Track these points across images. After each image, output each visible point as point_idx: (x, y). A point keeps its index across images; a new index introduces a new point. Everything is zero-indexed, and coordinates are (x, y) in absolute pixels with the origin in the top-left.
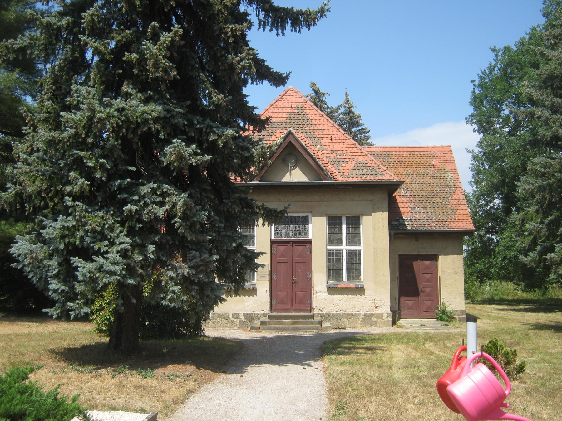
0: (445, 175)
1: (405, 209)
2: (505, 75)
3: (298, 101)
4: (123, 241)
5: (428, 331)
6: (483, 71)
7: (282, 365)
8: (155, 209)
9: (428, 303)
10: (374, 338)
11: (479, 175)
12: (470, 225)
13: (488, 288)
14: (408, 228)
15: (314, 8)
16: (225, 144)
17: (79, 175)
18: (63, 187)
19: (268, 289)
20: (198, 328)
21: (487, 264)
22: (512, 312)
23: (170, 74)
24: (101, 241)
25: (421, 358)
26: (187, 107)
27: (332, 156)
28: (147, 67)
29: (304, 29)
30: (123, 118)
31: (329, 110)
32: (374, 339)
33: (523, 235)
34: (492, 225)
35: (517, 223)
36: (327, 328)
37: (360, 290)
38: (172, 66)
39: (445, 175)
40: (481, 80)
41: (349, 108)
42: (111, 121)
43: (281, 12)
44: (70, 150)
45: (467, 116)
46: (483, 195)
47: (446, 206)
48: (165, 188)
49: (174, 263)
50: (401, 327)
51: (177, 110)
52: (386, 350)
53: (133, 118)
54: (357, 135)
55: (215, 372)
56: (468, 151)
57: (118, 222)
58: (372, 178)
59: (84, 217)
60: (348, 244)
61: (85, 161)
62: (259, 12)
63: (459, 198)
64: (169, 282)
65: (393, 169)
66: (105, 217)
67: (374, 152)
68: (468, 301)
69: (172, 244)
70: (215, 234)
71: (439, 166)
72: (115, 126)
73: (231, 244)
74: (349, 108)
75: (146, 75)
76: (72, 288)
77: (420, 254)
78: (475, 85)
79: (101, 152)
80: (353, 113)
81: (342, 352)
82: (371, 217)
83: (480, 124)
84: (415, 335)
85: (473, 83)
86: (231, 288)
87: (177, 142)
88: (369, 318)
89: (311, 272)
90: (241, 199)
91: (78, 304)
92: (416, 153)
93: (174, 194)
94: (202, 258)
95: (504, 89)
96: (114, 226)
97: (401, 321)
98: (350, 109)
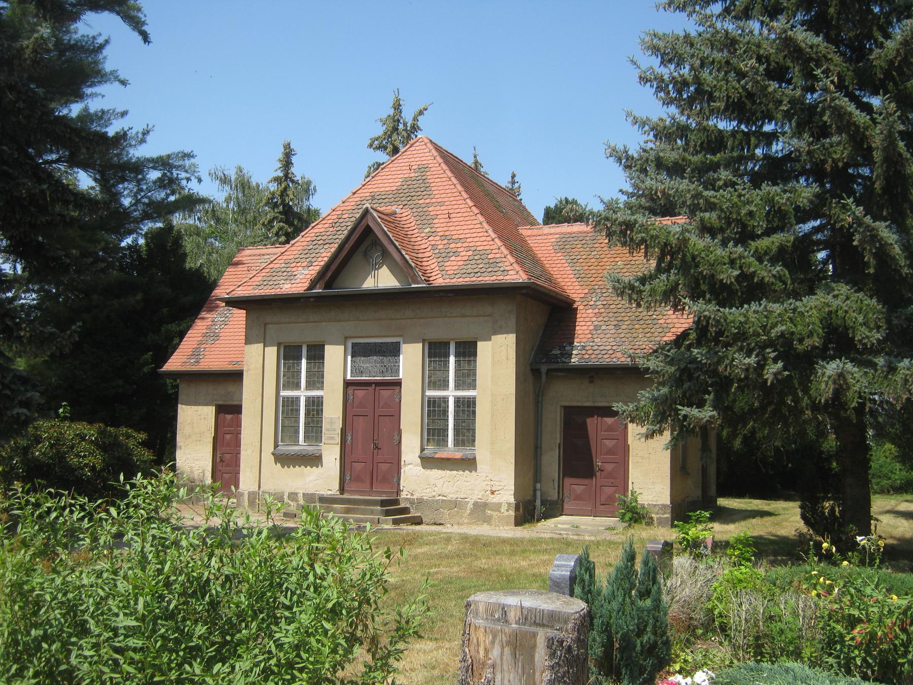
9: (608, 490)
19: (338, 457)
37: (469, 464)
47: (655, 322)
60: (458, 387)
67: (574, 233)
77: (596, 405)
82: (489, 343)
88: (481, 510)
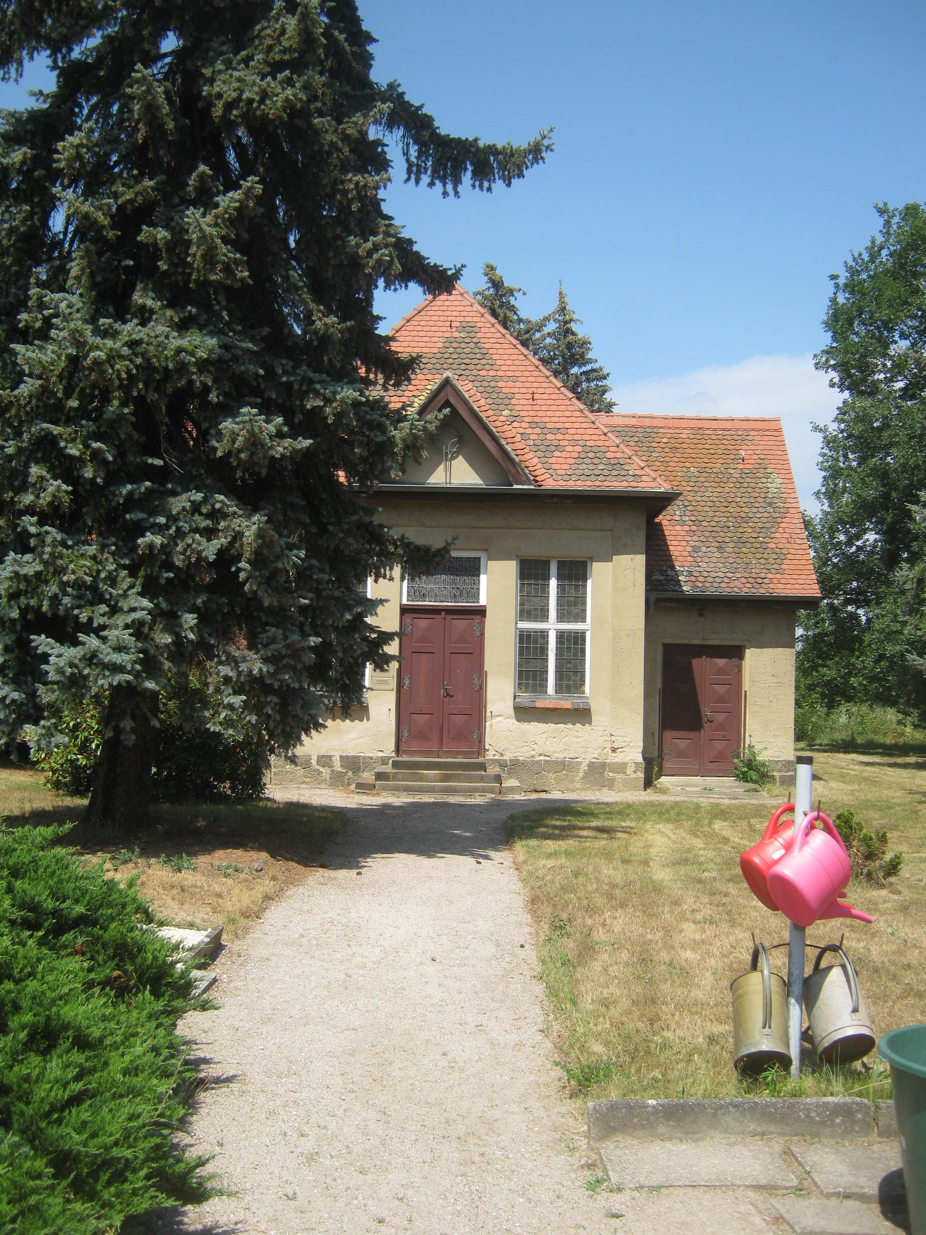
0: (766, 480)
1: (680, 548)
2: (903, 267)
3: (465, 314)
4: (136, 605)
5: (718, 801)
6: (856, 256)
7: (434, 856)
8: (199, 544)
9: (720, 745)
10: (609, 811)
11: (836, 479)
12: (812, 587)
13: (843, 719)
14: (685, 588)
15: (521, 142)
16: (339, 416)
17: (48, 472)
18: (16, 495)
20: (254, 781)
21: (844, 668)
22: (890, 769)
23: (235, 275)
24: (92, 604)
25: (704, 849)
26: (264, 339)
27: (534, 434)
28: (189, 259)
29: (499, 185)
30: (139, 361)
31: (522, 326)
32: (610, 813)
33: (918, 611)
34: (858, 587)
35: (907, 586)
36: (512, 790)
37: (582, 715)
38: (240, 260)
39: (766, 480)
40: (852, 276)
41: (566, 323)
42: (117, 367)
43: (453, 148)
44: (31, 422)
45: (818, 352)
46: (842, 522)
47: (764, 545)
48: (218, 501)
49: (232, 649)
50: (663, 791)
51: (244, 345)
52: (635, 834)
53: (159, 361)
54: (581, 383)
55: (306, 866)
56: (816, 429)
57: (124, 567)
58: (616, 484)
59: (61, 556)
60: (561, 618)
61: (63, 444)
62: (408, 145)
63: (791, 531)
64: (222, 687)
65: (657, 464)
66: (100, 556)
67: (619, 426)
68: (802, 744)
69: (228, 612)
70: (311, 595)
71: (753, 461)
72: (124, 376)
73: (342, 616)
74: (566, 323)
75: (183, 273)
76: (33, 695)
77: (707, 643)
78: (837, 286)
79: (94, 427)
80: (573, 334)
81: (550, 835)
82: (610, 564)
83: (844, 370)
84: (692, 807)
85: (834, 282)
86: (335, 703)
87: (250, 413)
89: (481, 674)
90: (360, 525)
91: (44, 727)
92: (707, 432)
93: (235, 513)
94: (289, 641)
95: (899, 298)
96: (117, 576)
97: (663, 779)
98: (568, 326)
